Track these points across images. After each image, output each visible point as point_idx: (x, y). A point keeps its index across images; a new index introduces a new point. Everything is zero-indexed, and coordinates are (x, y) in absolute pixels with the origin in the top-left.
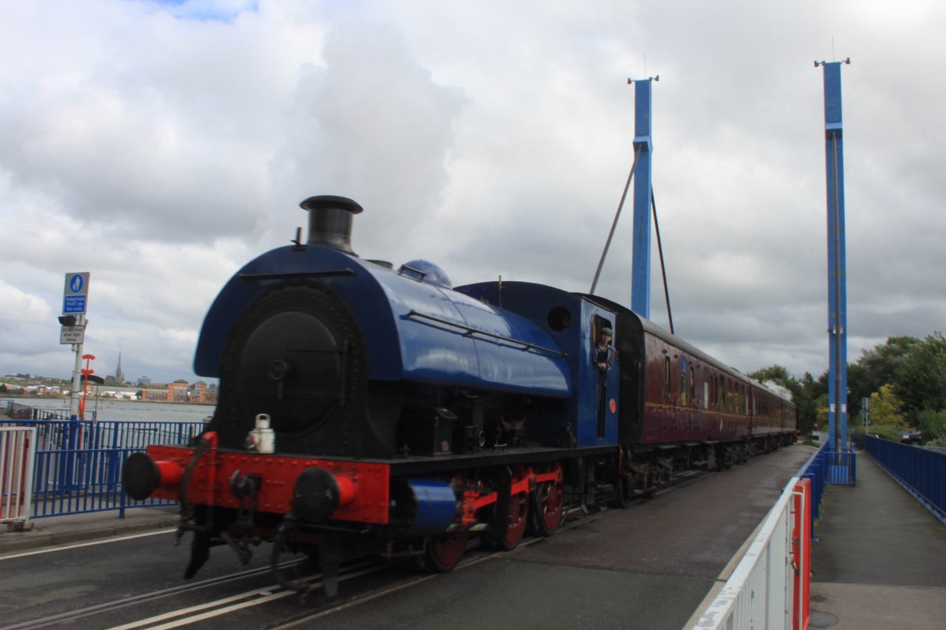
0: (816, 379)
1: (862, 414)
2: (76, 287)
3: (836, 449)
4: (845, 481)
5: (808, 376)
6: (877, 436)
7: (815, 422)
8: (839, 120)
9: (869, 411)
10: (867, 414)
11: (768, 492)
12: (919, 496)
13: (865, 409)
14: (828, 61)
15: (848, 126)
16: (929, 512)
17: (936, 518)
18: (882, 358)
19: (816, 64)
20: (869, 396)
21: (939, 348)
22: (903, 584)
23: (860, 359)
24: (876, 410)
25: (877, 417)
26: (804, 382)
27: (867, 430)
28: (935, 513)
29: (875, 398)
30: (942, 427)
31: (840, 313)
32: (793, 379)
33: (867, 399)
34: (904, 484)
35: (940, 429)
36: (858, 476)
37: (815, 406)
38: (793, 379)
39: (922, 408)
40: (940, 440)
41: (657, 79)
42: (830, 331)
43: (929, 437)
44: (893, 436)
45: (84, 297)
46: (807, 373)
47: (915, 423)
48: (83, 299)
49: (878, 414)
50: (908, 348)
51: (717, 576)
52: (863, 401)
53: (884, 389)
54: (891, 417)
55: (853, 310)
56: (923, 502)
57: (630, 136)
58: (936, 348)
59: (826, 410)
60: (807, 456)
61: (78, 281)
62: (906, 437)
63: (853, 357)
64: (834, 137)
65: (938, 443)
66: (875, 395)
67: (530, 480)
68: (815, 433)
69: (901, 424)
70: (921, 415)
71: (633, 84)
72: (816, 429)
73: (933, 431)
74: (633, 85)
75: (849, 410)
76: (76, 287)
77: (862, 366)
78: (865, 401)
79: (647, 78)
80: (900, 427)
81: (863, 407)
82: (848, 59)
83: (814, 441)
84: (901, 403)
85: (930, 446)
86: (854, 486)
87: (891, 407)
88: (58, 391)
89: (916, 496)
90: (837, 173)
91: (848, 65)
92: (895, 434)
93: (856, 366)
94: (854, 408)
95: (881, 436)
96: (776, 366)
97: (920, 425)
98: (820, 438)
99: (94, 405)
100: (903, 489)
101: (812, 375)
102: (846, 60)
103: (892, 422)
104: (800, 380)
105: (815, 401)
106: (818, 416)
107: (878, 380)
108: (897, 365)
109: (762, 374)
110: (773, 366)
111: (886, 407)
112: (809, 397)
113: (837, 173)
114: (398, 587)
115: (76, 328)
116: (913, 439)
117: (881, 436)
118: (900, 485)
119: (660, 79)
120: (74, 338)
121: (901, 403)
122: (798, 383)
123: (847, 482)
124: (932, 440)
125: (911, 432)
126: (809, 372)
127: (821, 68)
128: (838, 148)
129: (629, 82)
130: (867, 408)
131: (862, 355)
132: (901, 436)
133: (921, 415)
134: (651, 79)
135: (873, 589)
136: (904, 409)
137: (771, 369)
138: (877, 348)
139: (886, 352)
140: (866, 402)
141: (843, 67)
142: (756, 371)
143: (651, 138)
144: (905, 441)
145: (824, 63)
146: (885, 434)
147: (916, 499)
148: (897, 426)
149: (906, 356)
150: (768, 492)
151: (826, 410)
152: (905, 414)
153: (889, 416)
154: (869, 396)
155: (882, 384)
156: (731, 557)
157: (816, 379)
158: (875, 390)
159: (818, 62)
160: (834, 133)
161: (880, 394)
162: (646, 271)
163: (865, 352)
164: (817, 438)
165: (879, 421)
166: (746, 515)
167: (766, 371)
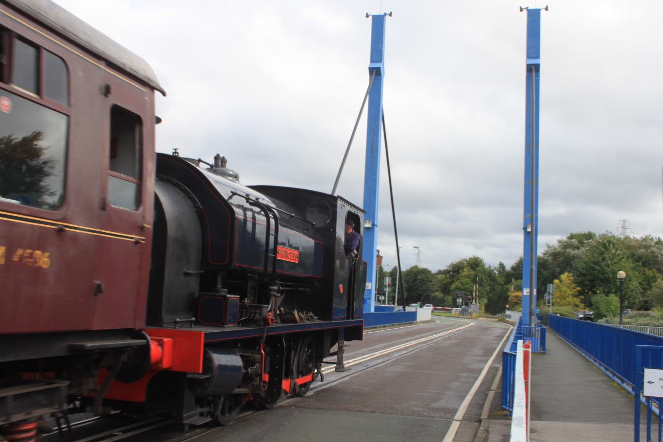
0: (508, 268)
1: (547, 297)
3: (530, 325)
4: (537, 350)
5: (502, 266)
6: (559, 315)
7: (507, 303)
9: (552, 294)
10: (551, 297)
11: (478, 358)
12: (595, 361)
13: (549, 293)
14: (530, 8)
15: (544, 61)
16: (603, 372)
17: (608, 376)
18: (562, 251)
19: (521, 10)
20: (552, 283)
21: (609, 245)
22: (589, 421)
23: (544, 252)
24: (557, 294)
25: (558, 300)
26: (498, 270)
27: (551, 310)
28: (608, 373)
29: (557, 284)
30: (610, 308)
31: (534, 215)
32: (490, 267)
33: (551, 285)
34: (582, 352)
35: (609, 309)
36: (547, 347)
37: (508, 290)
38: (490, 267)
39: (595, 293)
40: (608, 318)
41: (390, 15)
42: (525, 229)
43: (600, 316)
44: (571, 315)
46: (501, 263)
47: (589, 304)
49: (558, 297)
50: (584, 243)
51: (453, 417)
52: (548, 286)
53: (564, 276)
54: (570, 299)
55: (544, 211)
56: (598, 365)
57: (365, 63)
58: (607, 244)
59: (518, 294)
60: (503, 331)
62: (581, 316)
63: (540, 252)
64: (533, 70)
65: (607, 321)
66: (556, 281)
68: (508, 313)
69: (577, 306)
70: (594, 299)
71: (370, 18)
72: (508, 309)
73: (604, 311)
74: (370, 18)
77: (546, 258)
78: (550, 287)
79: (383, 14)
80: (576, 308)
81: (548, 291)
83: (507, 319)
84: (579, 289)
85: (601, 322)
86: (544, 353)
87: (569, 292)
89: (592, 361)
90: (534, 101)
91: (546, 11)
92: (573, 314)
93: (541, 258)
94: (541, 292)
95: (561, 315)
96: (474, 257)
97: (593, 306)
98: (512, 317)
100: (582, 356)
101: (505, 265)
102: (545, 7)
103: (569, 304)
104: (495, 268)
105: (506, 286)
106: (510, 298)
107: (558, 270)
108: (574, 257)
109: (464, 263)
110: (472, 257)
111: (565, 292)
112: (502, 283)
113: (534, 101)
116: (587, 318)
117: (561, 315)
118: (580, 354)
119: (393, 14)
121: (579, 289)
122: (587, 267)
123: (539, 351)
124: (602, 319)
125: (585, 312)
126: (502, 262)
127: (525, 12)
128: (536, 80)
129: (367, 16)
130: (551, 293)
131: (546, 249)
132: (577, 315)
133: (594, 299)
134: (385, 14)
135: (569, 425)
136: (580, 293)
137: (470, 259)
138: (560, 242)
139: (565, 246)
140: (551, 287)
141: (543, 13)
142: (459, 261)
143: (383, 64)
144: (581, 318)
145: (527, 9)
146: (565, 313)
147: (592, 363)
148: (573, 307)
149: (583, 249)
150: (478, 358)
151: (518, 294)
152: (582, 297)
153: (567, 299)
154: (552, 283)
155: (562, 272)
156: (461, 404)
157: (508, 268)
158: (557, 278)
159: (522, 8)
160: (533, 67)
161: (561, 282)
162: (376, 176)
163: (549, 247)
164: (509, 316)
165: (559, 303)
166: (464, 375)
167: (467, 261)
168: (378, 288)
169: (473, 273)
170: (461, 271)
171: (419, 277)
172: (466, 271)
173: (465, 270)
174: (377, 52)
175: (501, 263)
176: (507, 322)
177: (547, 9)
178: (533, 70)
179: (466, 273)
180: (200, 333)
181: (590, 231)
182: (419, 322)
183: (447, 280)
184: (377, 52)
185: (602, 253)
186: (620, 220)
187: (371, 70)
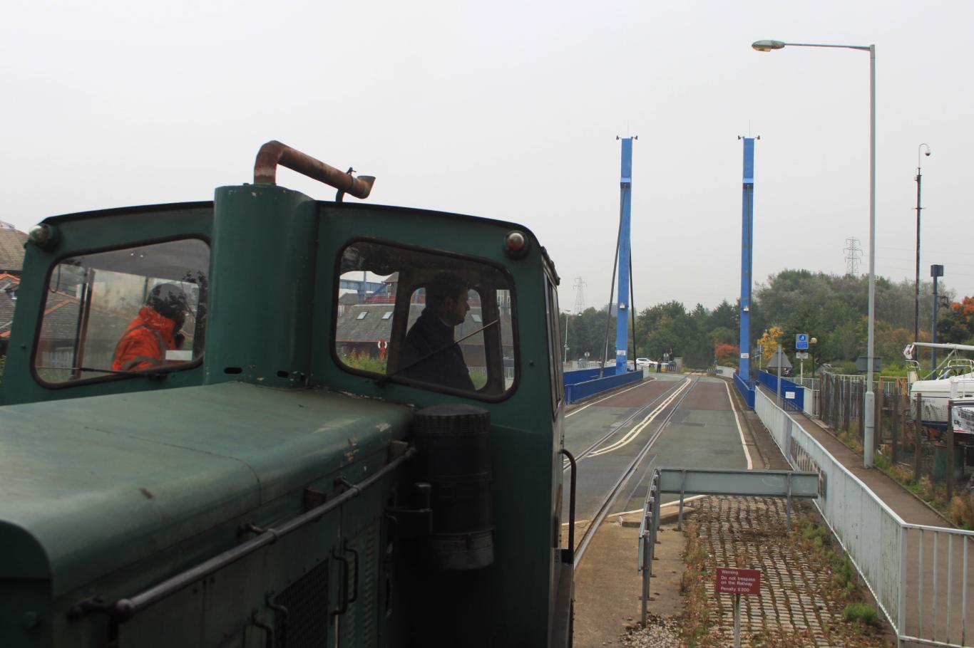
14: (747, 137)
15: (756, 181)
19: (739, 138)
41: (636, 138)
46: (699, 304)
79: (630, 138)
96: (674, 302)
129: (618, 138)
141: (756, 141)
164: (721, 372)
167: (664, 306)
168: (702, 369)
169: (673, 321)
170: (658, 318)
171: (597, 323)
172: (664, 320)
173: (664, 317)
174: (626, 170)
175: (699, 304)
176: (719, 377)
177: (759, 138)
178: (748, 188)
179: (665, 322)
180: (782, 379)
181: (804, 269)
182: (647, 378)
183: (640, 329)
184: (626, 170)
185: (803, 319)
186: (847, 239)
187: (622, 184)
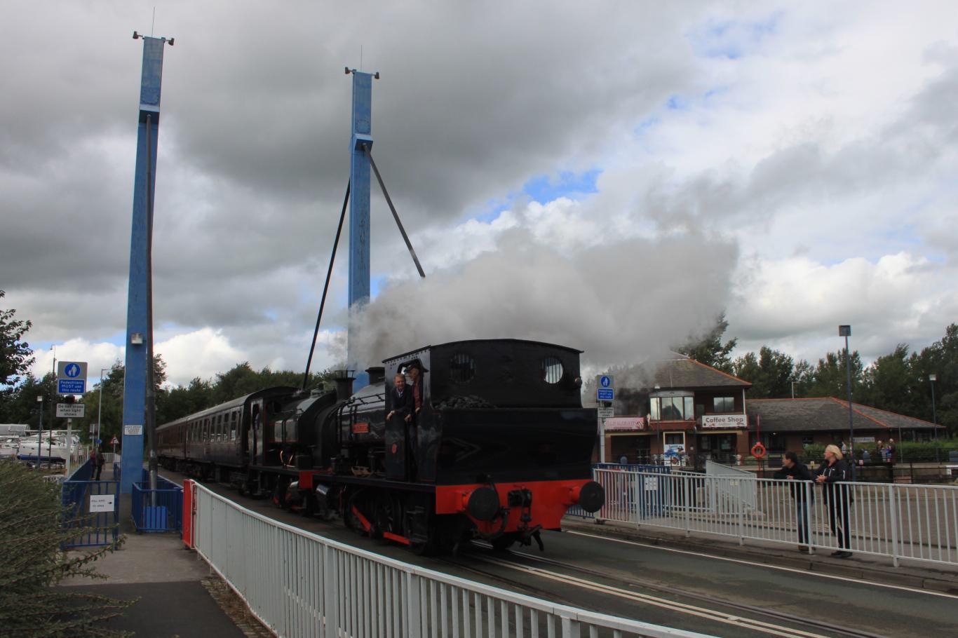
2: (72, 373)
5: (731, 351)
8: (157, 103)
19: (347, 71)
41: (171, 42)
45: (83, 381)
48: (82, 383)
61: (606, 380)
67: (426, 371)
74: (140, 41)
75: (718, 351)
76: (72, 373)
82: (173, 40)
88: (690, 412)
99: (42, 444)
114: (370, 411)
115: (75, 405)
120: (74, 413)
129: (136, 36)
134: (163, 40)
145: (354, 72)
160: (149, 115)
